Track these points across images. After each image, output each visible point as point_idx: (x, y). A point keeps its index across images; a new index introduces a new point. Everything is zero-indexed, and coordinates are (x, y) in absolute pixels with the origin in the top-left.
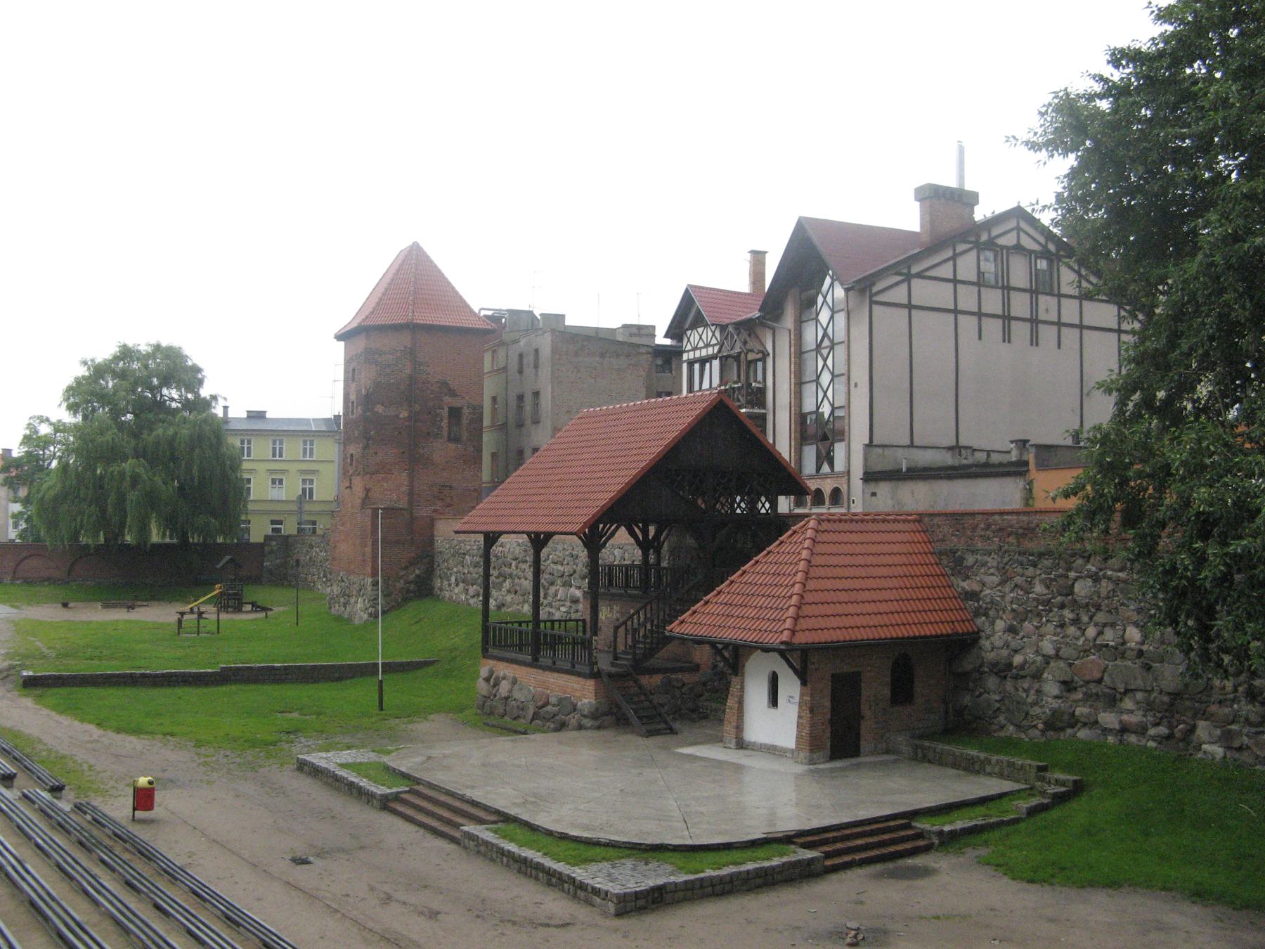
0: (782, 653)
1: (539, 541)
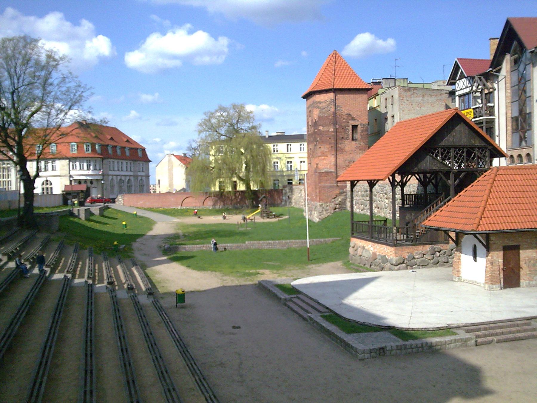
0: (474, 235)
1: (372, 184)
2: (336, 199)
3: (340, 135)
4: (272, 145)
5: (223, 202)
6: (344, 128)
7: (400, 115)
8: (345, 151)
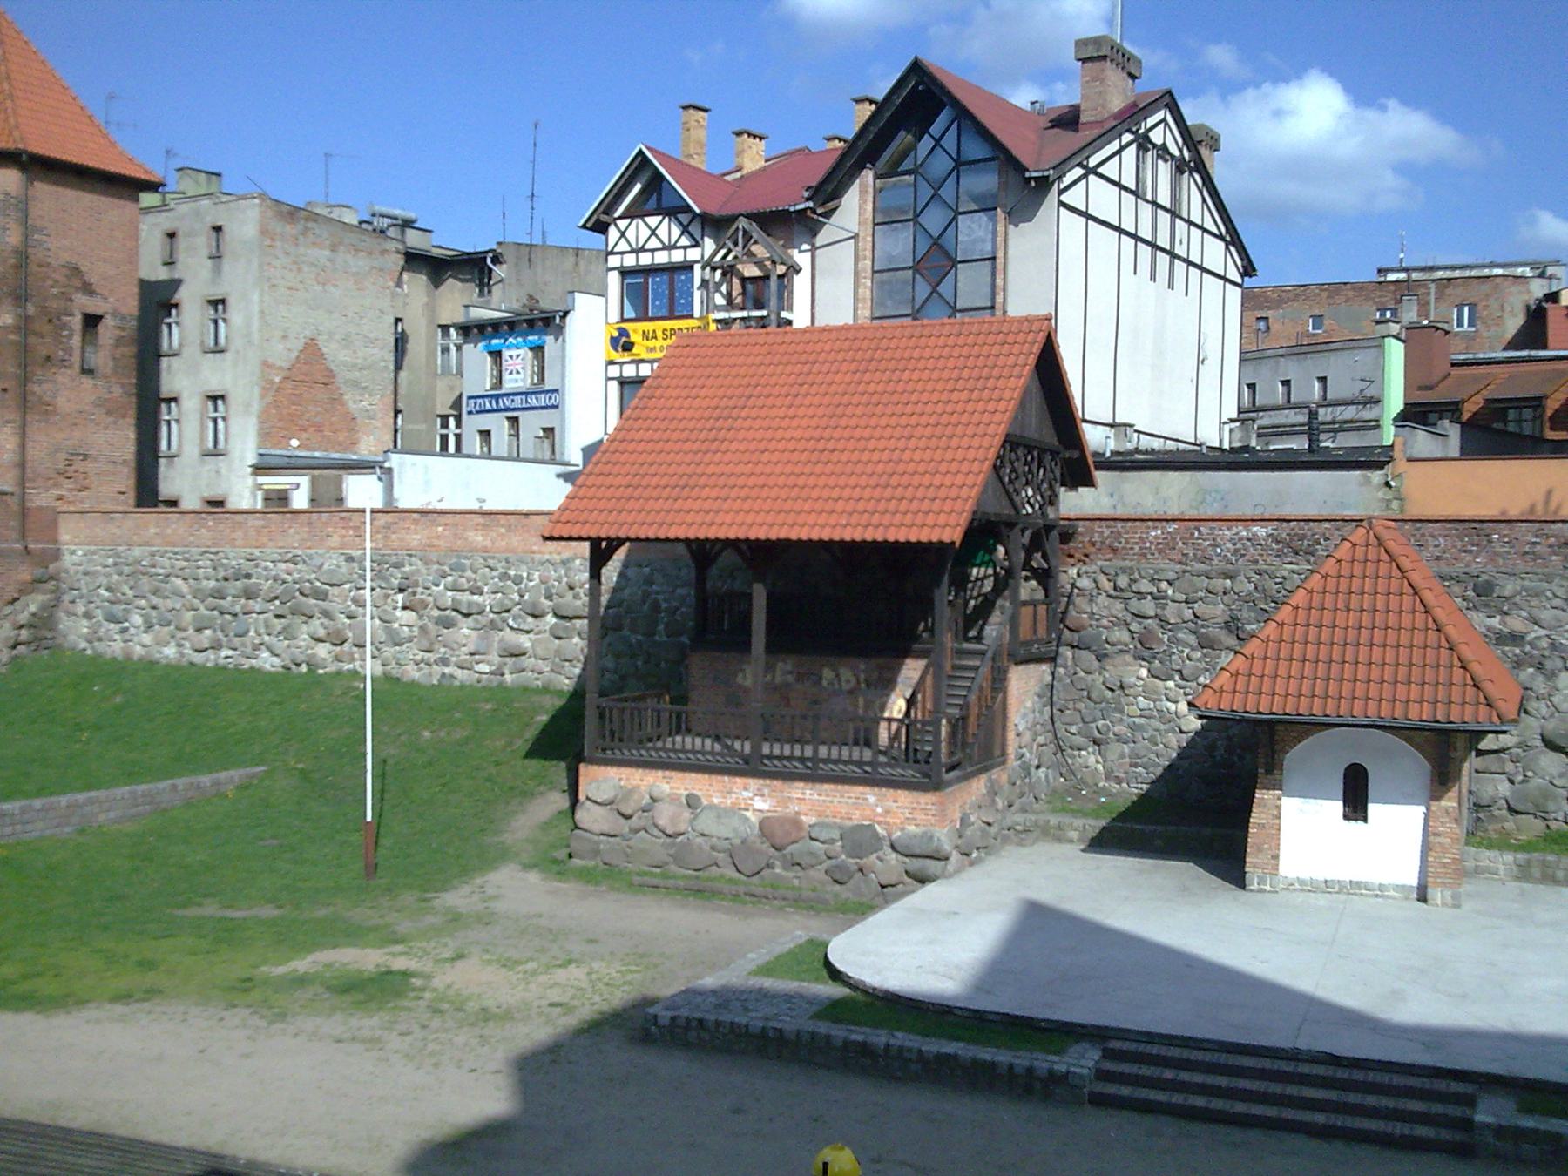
2: (18, 605)
3: (42, 347)
6: (55, 320)
7: (262, 301)
8: (55, 412)
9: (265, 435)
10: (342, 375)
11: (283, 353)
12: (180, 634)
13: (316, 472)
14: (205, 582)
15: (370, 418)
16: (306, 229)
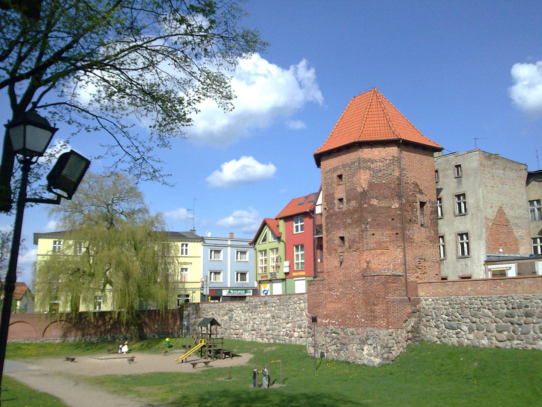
4: (180, 244)
5: (83, 329)
6: (411, 204)
7: (483, 193)
9: (488, 248)
10: (512, 221)
11: (491, 213)
12: (490, 334)
13: (520, 261)
14: (501, 310)
15: (522, 239)
16: (495, 162)
